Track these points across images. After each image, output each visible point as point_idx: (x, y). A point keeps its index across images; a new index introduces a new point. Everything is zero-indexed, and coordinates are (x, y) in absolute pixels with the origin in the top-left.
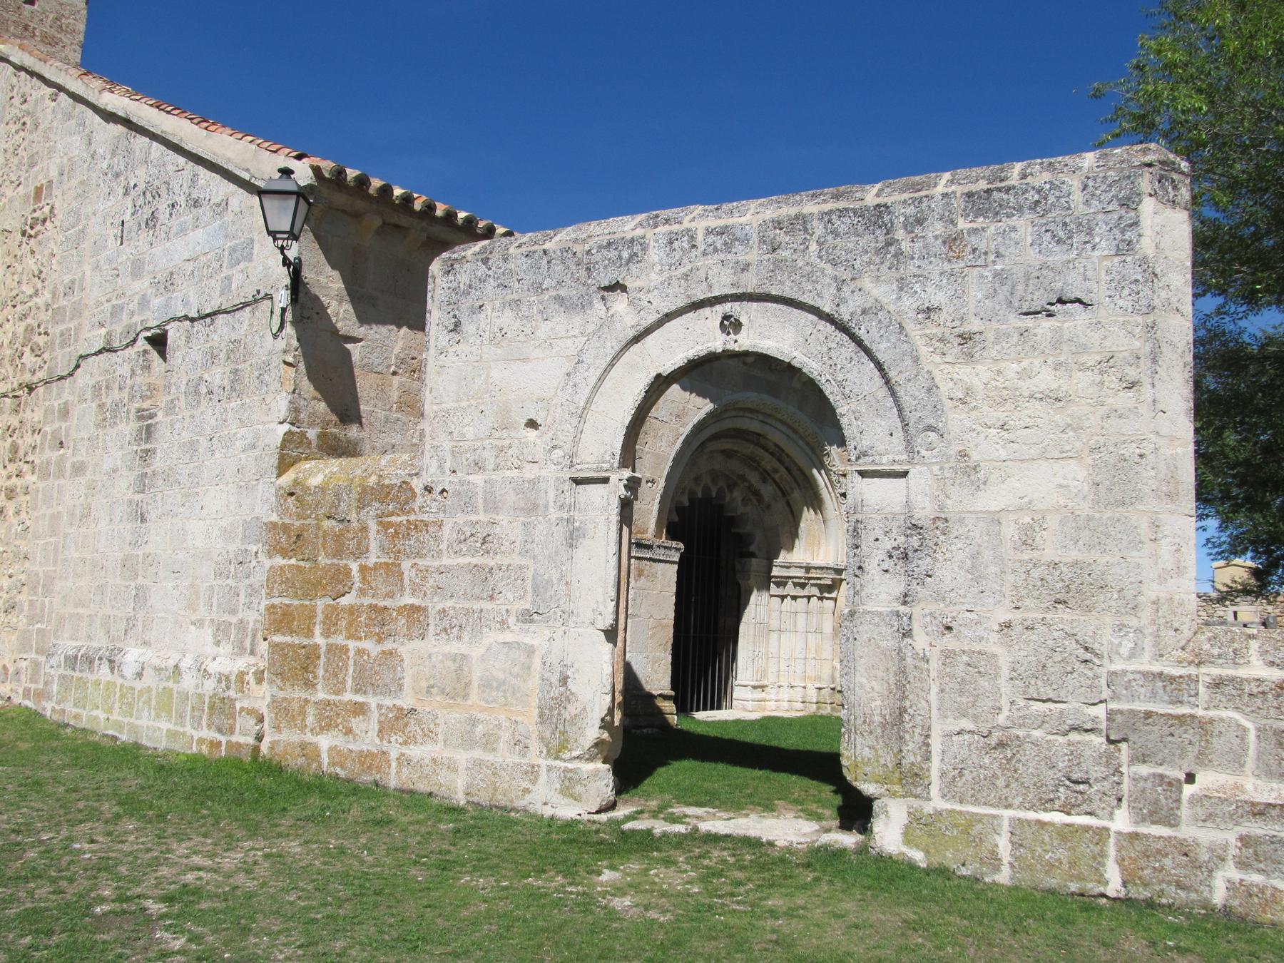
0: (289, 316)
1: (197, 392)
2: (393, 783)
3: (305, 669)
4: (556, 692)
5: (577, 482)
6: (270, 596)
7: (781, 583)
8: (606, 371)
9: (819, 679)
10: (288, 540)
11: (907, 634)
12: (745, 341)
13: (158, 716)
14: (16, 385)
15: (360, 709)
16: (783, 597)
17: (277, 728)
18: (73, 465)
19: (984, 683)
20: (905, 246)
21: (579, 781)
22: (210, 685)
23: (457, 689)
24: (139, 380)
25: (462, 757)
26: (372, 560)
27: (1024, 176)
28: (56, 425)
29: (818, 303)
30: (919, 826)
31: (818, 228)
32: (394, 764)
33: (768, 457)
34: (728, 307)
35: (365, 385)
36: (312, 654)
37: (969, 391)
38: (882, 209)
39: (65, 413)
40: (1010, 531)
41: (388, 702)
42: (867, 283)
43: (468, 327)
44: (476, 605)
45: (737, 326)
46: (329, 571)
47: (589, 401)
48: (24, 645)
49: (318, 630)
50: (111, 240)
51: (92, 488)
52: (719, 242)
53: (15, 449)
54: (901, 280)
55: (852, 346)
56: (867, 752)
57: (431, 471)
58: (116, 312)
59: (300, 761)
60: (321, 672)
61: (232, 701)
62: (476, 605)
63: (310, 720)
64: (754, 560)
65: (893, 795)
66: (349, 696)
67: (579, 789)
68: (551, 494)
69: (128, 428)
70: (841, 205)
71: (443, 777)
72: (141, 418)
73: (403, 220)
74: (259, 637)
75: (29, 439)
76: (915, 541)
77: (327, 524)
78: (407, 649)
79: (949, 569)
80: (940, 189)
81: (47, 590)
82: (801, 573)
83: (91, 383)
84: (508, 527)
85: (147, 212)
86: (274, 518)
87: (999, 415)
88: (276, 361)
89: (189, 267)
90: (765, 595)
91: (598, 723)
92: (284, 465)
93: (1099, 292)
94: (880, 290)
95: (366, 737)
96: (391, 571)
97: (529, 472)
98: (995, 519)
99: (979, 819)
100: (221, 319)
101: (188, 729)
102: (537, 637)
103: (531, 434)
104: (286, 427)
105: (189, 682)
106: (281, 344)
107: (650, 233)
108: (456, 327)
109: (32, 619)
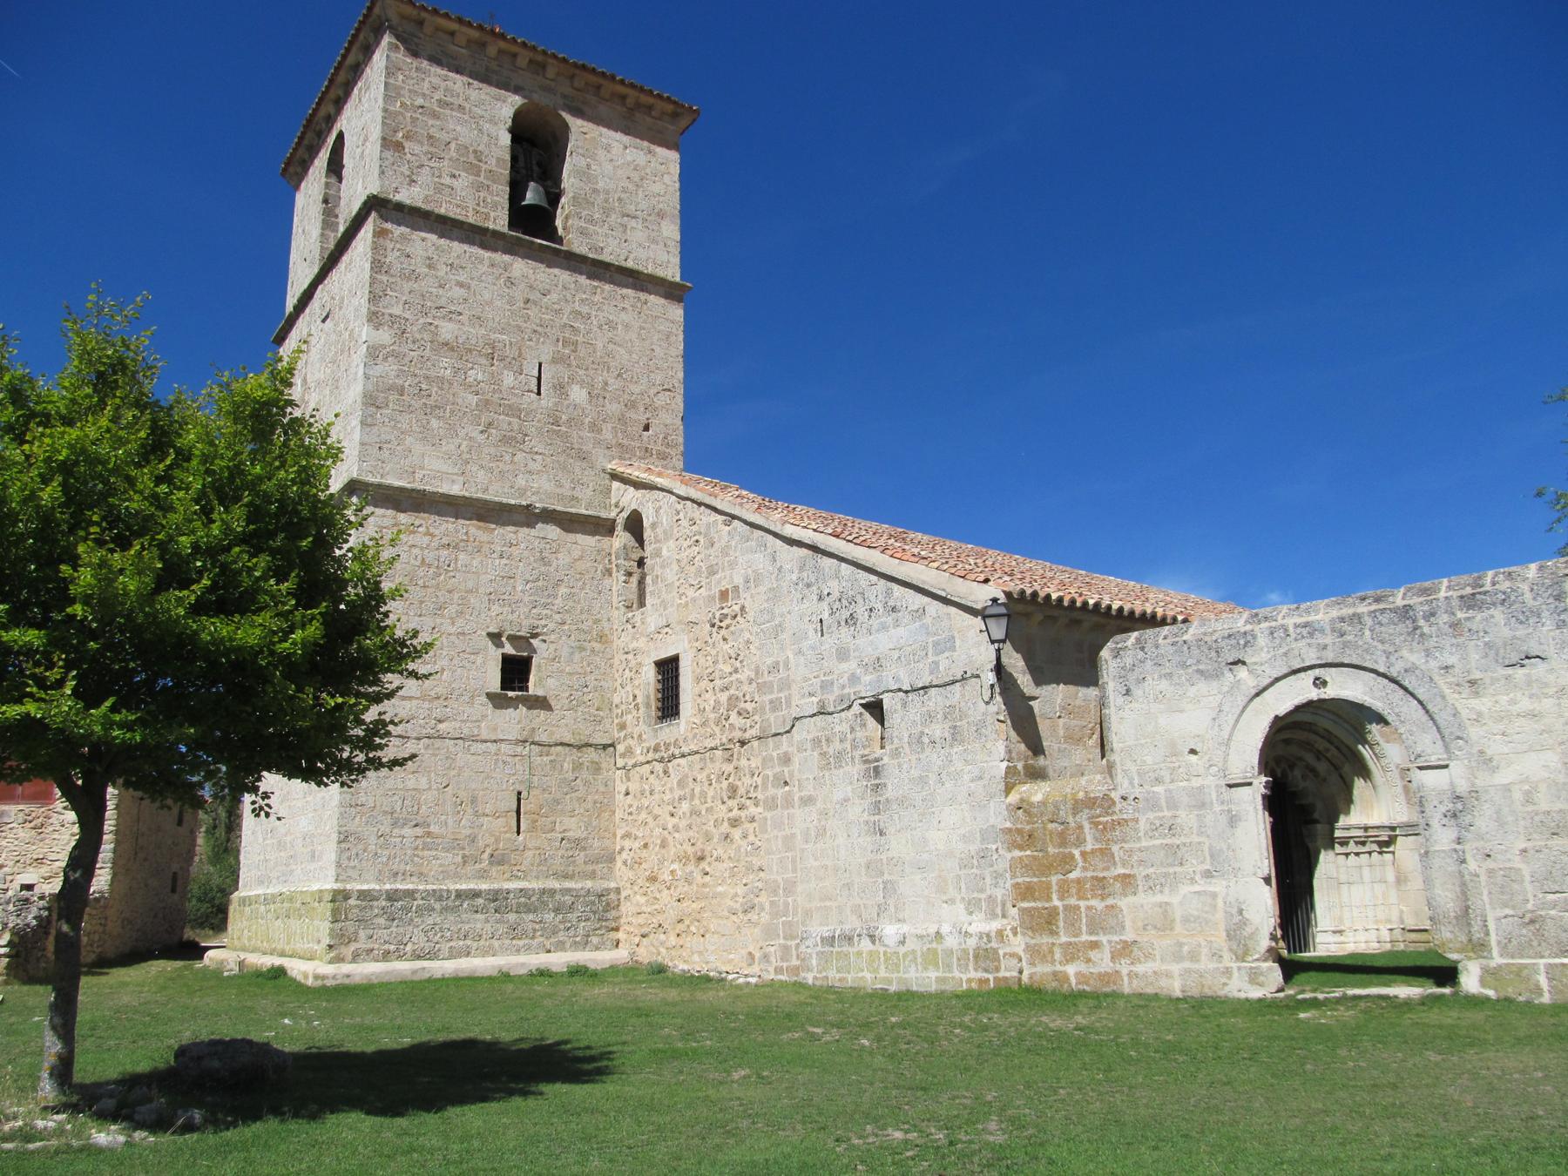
0: (997, 689)
1: (920, 742)
2: (1127, 990)
3: (1049, 923)
4: (1237, 919)
5: (1230, 786)
6: (1013, 876)
7: (1344, 842)
8: (1240, 715)
9: (1390, 921)
10: (1023, 838)
11: (1464, 861)
12: (1330, 692)
13: (926, 969)
14: (725, 740)
15: (1095, 945)
16: (1347, 855)
17: (1033, 964)
18: (801, 798)
19: (1516, 886)
20: (1426, 630)
21: (1262, 974)
22: (972, 943)
23: (1164, 922)
24: (859, 735)
25: (1176, 968)
26: (1089, 848)
27: (1494, 584)
28: (778, 769)
29: (1376, 667)
30: (1489, 976)
31: (1369, 621)
32: (1126, 979)
33: (1319, 740)
34: (1317, 672)
35: (1043, 727)
36: (1052, 914)
37: (1480, 714)
38: (1408, 608)
39: (786, 759)
40: (1517, 795)
41: (1116, 938)
42: (1405, 653)
43: (1137, 692)
44: (1171, 870)
45: (1325, 683)
46: (1054, 855)
47: (1231, 735)
48: (770, 932)
49: (1054, 896)
50: (811, 633)
51: (824, 814)
52: (1305, 631)
53: (733, 790)
54: (1427, 650)
55: (1401, 692)
56: (1448, 935)
57: (1123, 786)
58: (825, 686)
59: (1054, 984)
60: (1061, 924)
61: (995, 951)
62: (1171, 870)
63: (1057, 956)
64: (1319, 826)
65: (1470, 958)
66: (1085, 937)
67: (1262, 978)
68: (1214, 796)
69: (856, 769)
70: (1382, 606)
71: (1164, 983)
72: (866, 762)
73: (1056, 613)
74: (1009, 905)
75: (747, 780)
76: (1459, 806)
77: (1051, 826)
78: (1124, 903)
79: (1483, 820)
80: (1442, 594)
81: (790, 888)
82: (1360, 833)
83: (810, 737)
84: (1186, 818)
85: (845, 614)
86: (1008, 825)
87: (1501, 727)
88: (990, 720)
89: (896, 655)
90: (1331, 853)
91: (1267, 936)
92: (1008, 790)
93: (1550, 651)
94: (1414, 657)
95: (1102, 962)
96: (1105, 853)
97: (1196, 783)
98: (1507, 788)
99: (1525, 966)
100: (933, 691)
101: (957, 974)
102: (1217, 886)
103: (1193, 758)
104: (1005, 764)
105: (952, 942)
106: (993, 708)
107: (1257, 628)
108: (1128, 692)
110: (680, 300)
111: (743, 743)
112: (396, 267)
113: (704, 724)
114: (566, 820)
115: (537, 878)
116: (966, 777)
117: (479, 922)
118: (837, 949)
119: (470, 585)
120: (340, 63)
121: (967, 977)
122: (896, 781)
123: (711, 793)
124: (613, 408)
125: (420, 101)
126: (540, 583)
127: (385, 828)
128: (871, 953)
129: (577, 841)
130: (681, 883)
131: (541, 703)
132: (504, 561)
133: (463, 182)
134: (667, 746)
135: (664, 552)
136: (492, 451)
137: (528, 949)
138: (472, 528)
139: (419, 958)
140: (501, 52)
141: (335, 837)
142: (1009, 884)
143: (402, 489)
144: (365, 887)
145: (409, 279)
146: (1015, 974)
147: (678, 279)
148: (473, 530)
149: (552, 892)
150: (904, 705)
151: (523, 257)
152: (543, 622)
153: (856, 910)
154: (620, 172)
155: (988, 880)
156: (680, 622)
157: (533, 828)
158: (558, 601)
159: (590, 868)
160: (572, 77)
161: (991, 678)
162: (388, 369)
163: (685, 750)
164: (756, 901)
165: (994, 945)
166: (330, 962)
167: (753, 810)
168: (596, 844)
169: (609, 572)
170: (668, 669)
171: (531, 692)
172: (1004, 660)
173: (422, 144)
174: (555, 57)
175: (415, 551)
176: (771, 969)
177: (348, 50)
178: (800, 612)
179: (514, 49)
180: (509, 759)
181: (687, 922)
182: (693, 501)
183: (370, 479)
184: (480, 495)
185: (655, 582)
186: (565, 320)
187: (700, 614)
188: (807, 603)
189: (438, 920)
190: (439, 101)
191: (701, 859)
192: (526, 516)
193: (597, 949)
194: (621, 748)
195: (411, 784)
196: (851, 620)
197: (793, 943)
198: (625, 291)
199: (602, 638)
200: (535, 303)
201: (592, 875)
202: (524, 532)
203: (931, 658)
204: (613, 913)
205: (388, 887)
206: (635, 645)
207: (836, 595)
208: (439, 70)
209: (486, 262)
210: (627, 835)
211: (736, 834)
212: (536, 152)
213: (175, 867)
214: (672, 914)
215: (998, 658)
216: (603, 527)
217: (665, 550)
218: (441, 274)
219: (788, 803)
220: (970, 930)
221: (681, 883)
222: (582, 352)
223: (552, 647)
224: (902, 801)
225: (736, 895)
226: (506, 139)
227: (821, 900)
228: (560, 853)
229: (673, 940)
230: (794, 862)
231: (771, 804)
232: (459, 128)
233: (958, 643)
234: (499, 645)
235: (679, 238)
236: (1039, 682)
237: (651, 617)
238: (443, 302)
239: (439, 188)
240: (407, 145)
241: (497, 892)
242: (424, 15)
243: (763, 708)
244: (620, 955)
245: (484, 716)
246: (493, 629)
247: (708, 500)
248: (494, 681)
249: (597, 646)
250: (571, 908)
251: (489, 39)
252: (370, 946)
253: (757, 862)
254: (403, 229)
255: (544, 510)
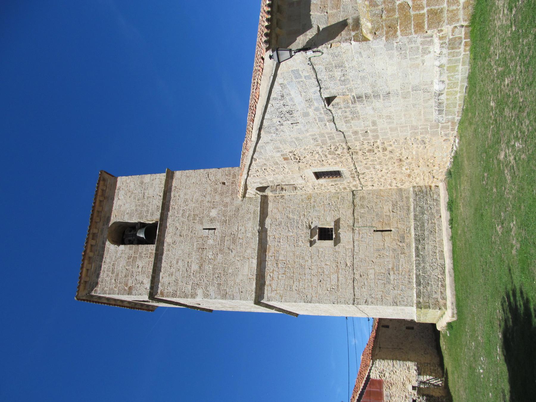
0: (315, 49)
1: (344, 81)
6: (411, 34)
13: (457, 71)
17: (458, 21)
18: (373, 126)
22: (445, 51)
24: (342, 106)
28: (360, 135)
35: (333, 21)
36: (430, 12)
39: (356, 133)
48: (435, 134)
49: (422, 12)
50: (297, 127)
51: (380, 117)
53: (370, 151)
58: (321, 120)
59: (470, 8)
60: (437, 7)
63: (454, 8)
69: (359, 106)
73: (275, 21)
74: (426, 35)
75: (366, 146)
77: (384, 17)
81: (416, 128)
83: (345, 124)
85: (287, 115)
86: (384, 38)
88: (331, 51)
89: (303, 94)
92: (366, 40)
100: (319, 77)
101: (461, 57)
104: (352, 42)
105: (444, 60)
106: (325, 51)
109: (427, 132)
110: (173, 173)
111: (349, 148)
112: (174, 288)
113: (342, 162)
114: (385, 210)
115: (409, 222)
116: (360, 59)
117: (429, 247)
118: (445, 108)
119: (291, 254)
120: (107, 304)
121: (463, 52)
122: (364, 89)
123: (372, 158)
124: (218, 198)
125: (113, 281)
126: (289, 225)
127: (391, 287)
128: (447, 95)
129: (393, 205)
130: (411, 166)
131: (337, 223)
132: (281, 241)
133: (140, 263)
134: (351, 174)
135: (271, 179)
136: (238, 247)
137: (439, 225)
138: (269, 254)
139: (444, 272)
140: (91, 251)
141: (395, 307)
142: (414, 35)
143: (256, 284)
144: (415, 295)
145: (177, 283)
146: (463, 29)
147: (165, 174)
148: (270, 254)
149: (415, 216)
150: (327, 89)
151: (164, 238)
152: (304, 223)
153: (426, 101)
154: (128, 201)
155: (413, 45)
156: (299, 173)
157: (389, 225)
158: (295, 217)
159: (405, 199)
160: (96, 222)
161: (310, 53)
162: (212, 290)
163: (353, 168)
164: (420, 140)
165: (447, 41)
166: (446, 309)
167: (379, 143)
168: (394, 197)
169: (282, 197)
170: (318, 175)
171: (333, 227)
172: (300, 47)
173: (128, 280)
174: (89, 230)
175: (280, 277)
176: (452, 132)
177: (102, 303)
178: (288, 132)
179: (89, 246)
180: (361, 236)
181: (429, 163)
182: (248, 172)
183: (254, 296)
184: (256, 252)
185: (284, 182)
186: (186, 220)
187: (296, 166)
188: (285, 129)
189: (428, 264)
190: (112, 273)
191: (401, 160)
192: (263, 232)
193: (439, 195)
194: (354, 189)
195: (372, 276)
196: (290, 112)
197: (440, 125)
198: (172, 196)
199: (309, 198)
200: (181, 232)
201: (408, 198)
202: (269, 233)
203: (303, 79)
204: (424, 188)
205: (415, 286)
206: (311, 187)
207: (279, 119)
208: (101, 274)
209: (168, 253)
210: (391, 185)
211: (389, 148)
212: (126, 234)
213: (404, 328)
214: (425, 169)
215: (299, 50)
216: (264, 201)
217: (269, 179)
218: (174, 270)
219: (375, 131)
220: (438, 52)
221: (411, 166)
222: (197, 212)
223: (314, 219)
224: (373, 86)
225: (417, 147)
226: (122, 247)
227: (420, 115)
228: (399, 212)
229: (437, 168)
230: (402, 127)
231: (376, 137)
232: (121, 266)
233: (294, 68)
234: (315, 242)
235: (150, 175)
236: (310, 27)
237: (299, 182)
238: (185, 270)
239: (143, 272)
240: (129, 285)
241: (416, 240)
242: (82, 281)
243: (333, 143)
244: (442, 187)
245: (344, 247)
246: (309, 245)
247: (247, 167)
248: (329, 243)
249: (312, 200)
250: (422, 207)
251: (87, 256)
252: (439, 293)
253: (402, 140)
254: (160, 286)
255: (260, 225)
